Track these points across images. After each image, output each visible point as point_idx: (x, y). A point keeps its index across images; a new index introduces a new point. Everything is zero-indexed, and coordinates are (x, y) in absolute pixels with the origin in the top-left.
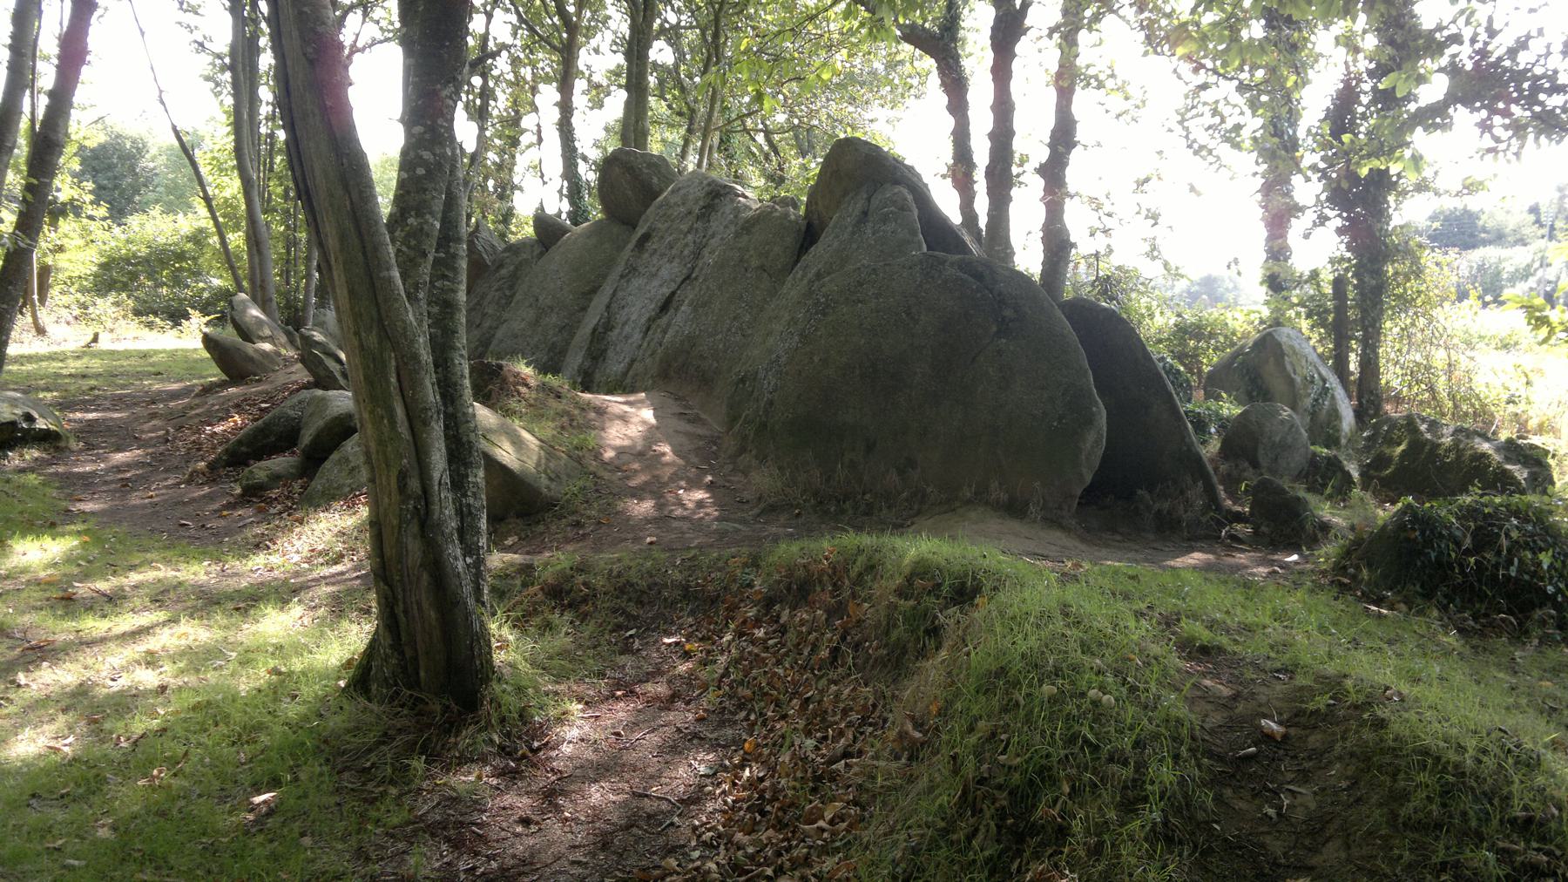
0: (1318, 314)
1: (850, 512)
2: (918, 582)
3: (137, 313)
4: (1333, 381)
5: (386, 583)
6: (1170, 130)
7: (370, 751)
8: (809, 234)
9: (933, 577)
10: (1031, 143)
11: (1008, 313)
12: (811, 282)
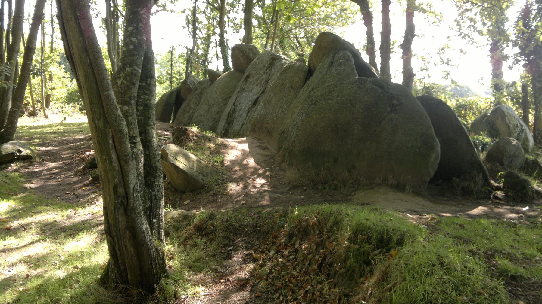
1: (328, 188)
4: (525, 127)
5: (111, 236)
6: (452, 29)
8: (310, 72)
9: (367, 233)
10: (397, 36)
11: (395, 102)
12: (310, 92)
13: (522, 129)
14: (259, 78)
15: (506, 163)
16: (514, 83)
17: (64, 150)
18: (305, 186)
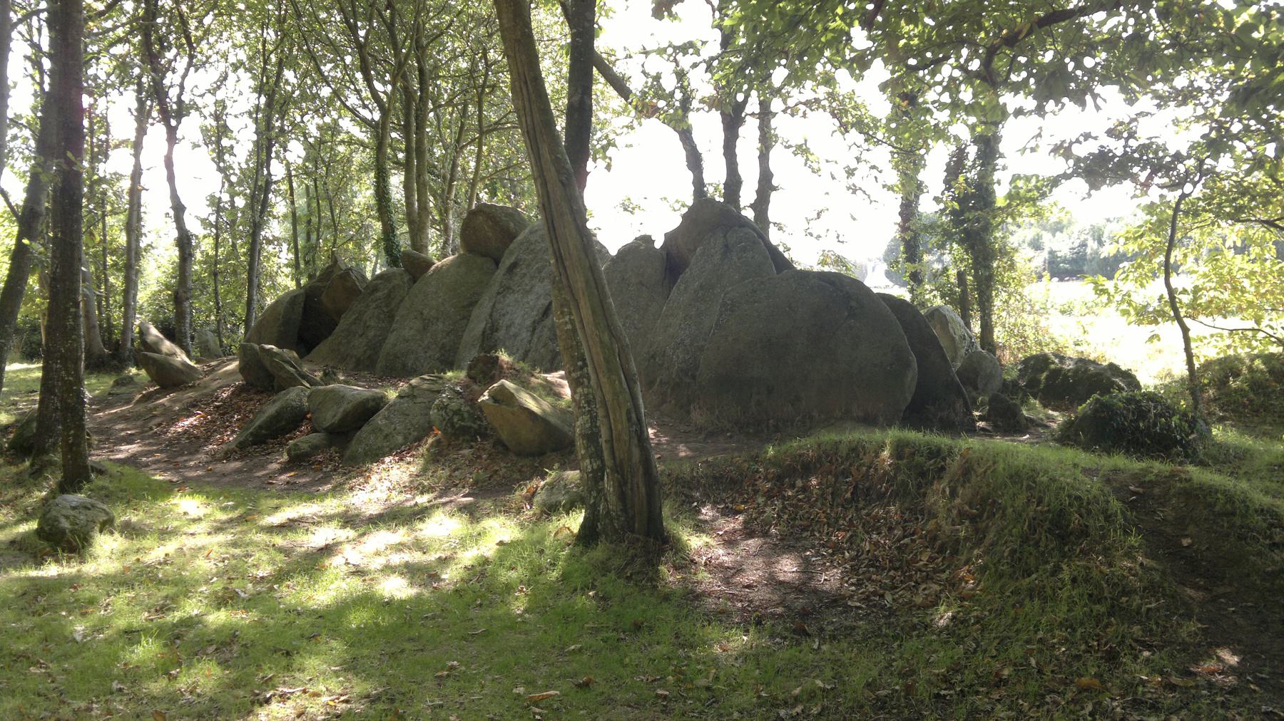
11: (853, 304)
15: (980, 386)
18: (728, 431)
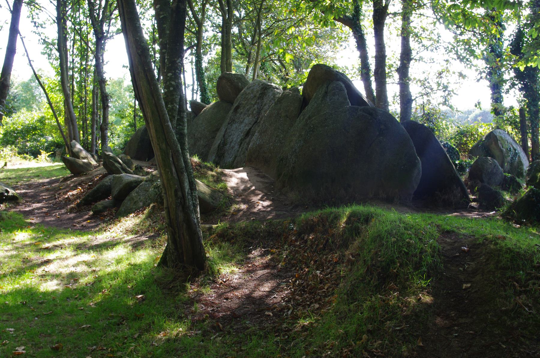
0: (514, 124)
2: (352, 218)
3: (19, 153)
4: (520, 150)
7: (170, 283)
8: (305, 101)
11: (382, 127)
13: (515, 152)
14: (250, 108)
16: (511, 108)
17: (42, 192)
